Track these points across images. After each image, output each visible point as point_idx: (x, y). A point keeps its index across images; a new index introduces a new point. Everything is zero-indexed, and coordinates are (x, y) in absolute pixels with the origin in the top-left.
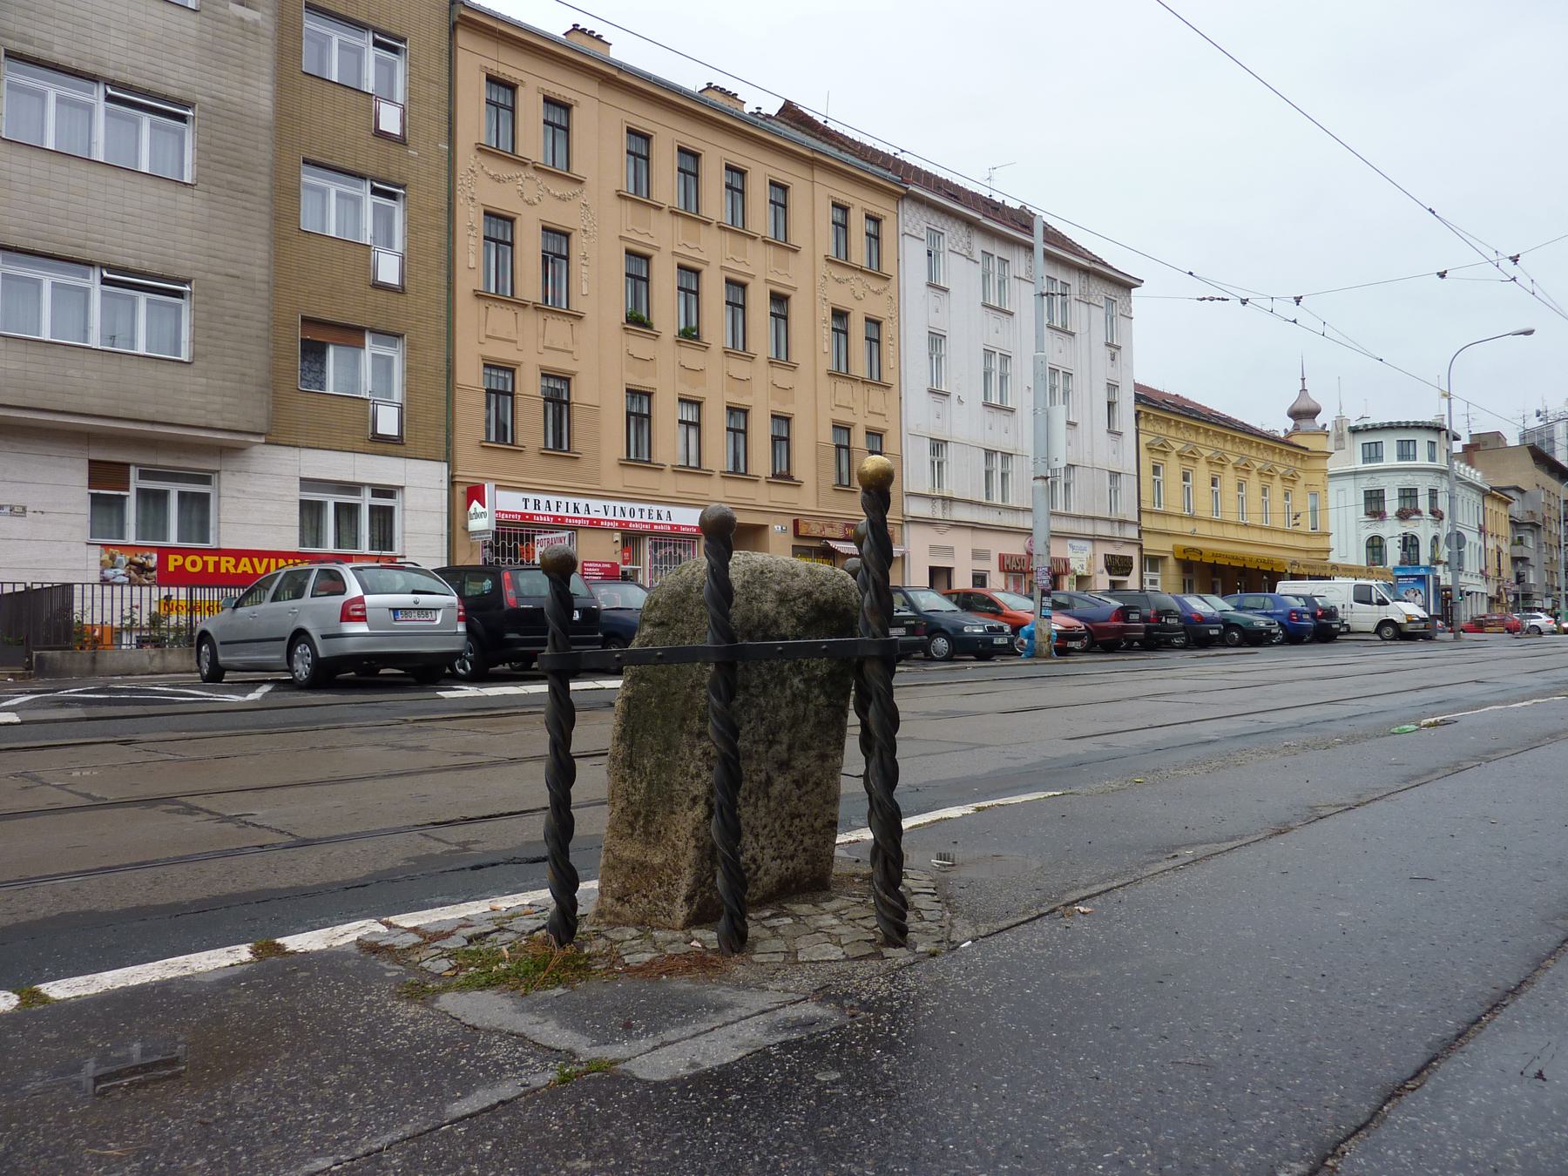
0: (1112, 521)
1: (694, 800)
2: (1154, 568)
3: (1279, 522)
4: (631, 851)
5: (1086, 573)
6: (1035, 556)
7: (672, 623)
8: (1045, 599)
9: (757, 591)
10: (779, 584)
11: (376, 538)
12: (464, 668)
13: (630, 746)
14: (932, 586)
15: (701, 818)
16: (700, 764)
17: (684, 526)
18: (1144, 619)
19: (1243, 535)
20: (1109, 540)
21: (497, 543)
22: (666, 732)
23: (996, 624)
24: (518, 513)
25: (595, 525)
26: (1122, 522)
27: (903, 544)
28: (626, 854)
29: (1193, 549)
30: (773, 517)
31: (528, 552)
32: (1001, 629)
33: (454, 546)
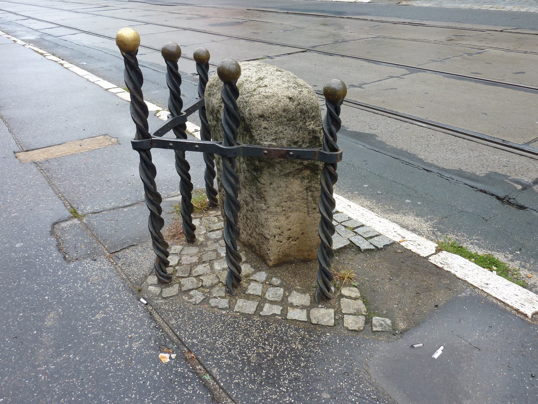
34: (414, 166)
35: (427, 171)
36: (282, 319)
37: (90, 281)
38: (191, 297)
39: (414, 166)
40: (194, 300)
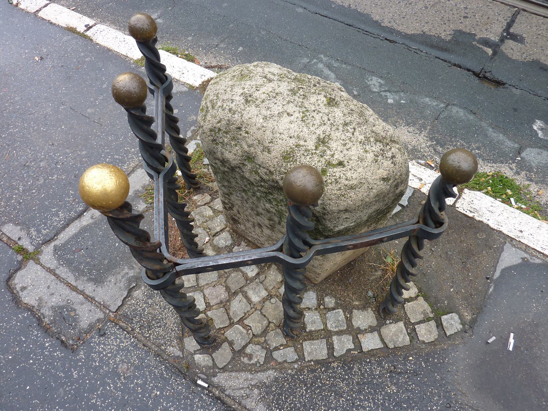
34: (373, 36)
35: (390, 41)
36: (359, 353)
38: (250, 357)
39: (373, 36)
40: (256, 360)
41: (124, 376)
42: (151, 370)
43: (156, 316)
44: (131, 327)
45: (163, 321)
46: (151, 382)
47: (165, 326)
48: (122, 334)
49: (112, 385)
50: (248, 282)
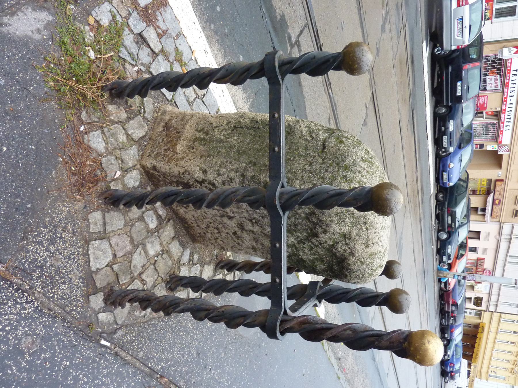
0: (497, 302)
1: (205, 172)
2: (476, 314)
3: (493, 363)
4: (189, 132)
5: (475, 289)
6: (480, 275)
7: (324, 155)
8: (462, 277)
9: (347, 220)
10: (357, 234)
11: (503, 10)
12: (438, 51)
13: (247, 128)
14: (470, 231)
15: (195, 176)
16: (226, 176)
17: (502, 136)
18: (453, 312)
19: (487, 358)
20: (489, 300)
21: (497, 60)
22: (249, 152)
23: (452, 257)
24: (511, 68)
25: (504, 99)
26: (496, 306)
27: (491, 222)
28: (188, 127)
29: (483, 330)
30: (505, 171)
31: (493, 73)
32: (449, 259)
33: (496, 43)
37: (25, 353)
41: (29, 352)
42: (60, 339)
43: (59, 268)
44: (29, 285)
45: (68, 275)
46: (60, 353)
47: (70, 281)
48: (23, 297)
49: (14, 368)
50: (149, 234)
